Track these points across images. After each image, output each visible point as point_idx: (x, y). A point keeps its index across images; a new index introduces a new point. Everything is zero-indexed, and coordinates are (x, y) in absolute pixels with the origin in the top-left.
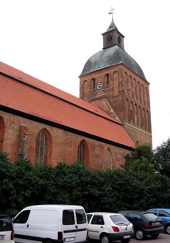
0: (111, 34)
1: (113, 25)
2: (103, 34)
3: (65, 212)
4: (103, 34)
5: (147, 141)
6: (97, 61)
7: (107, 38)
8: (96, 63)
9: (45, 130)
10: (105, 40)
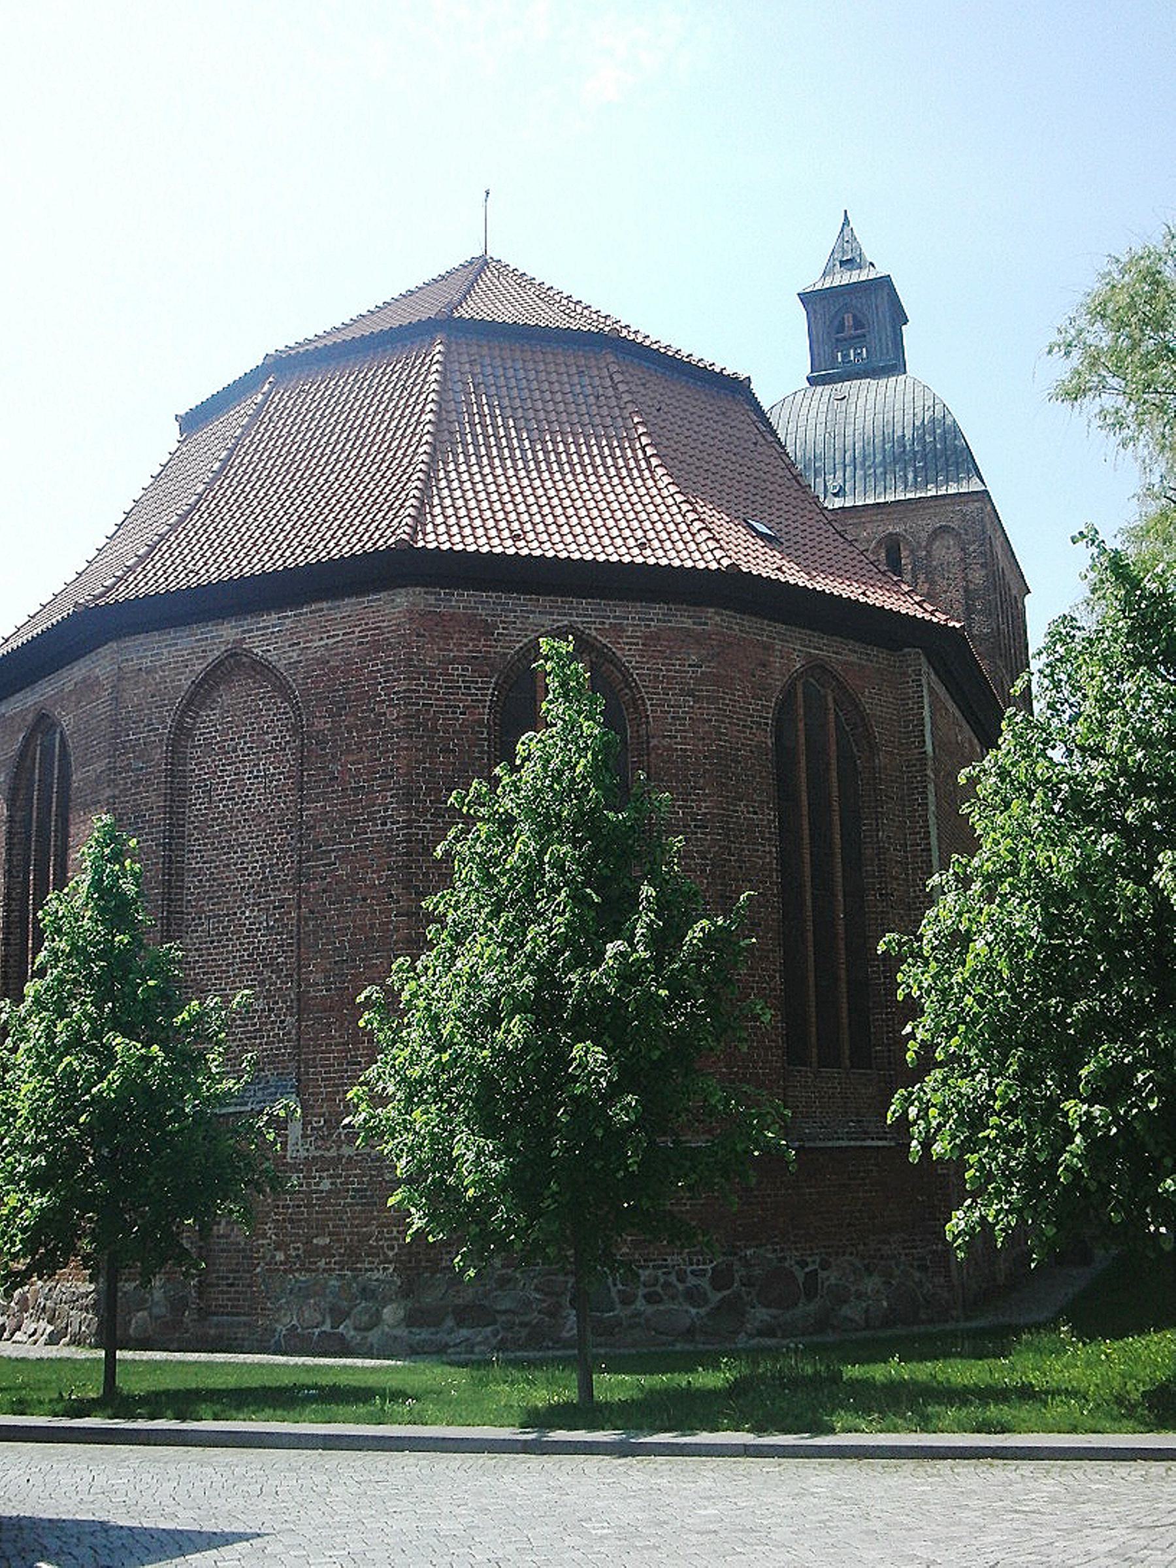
2: (806, 298)
4: (806, 298)
7: (834, 317)
9: (817, 669)
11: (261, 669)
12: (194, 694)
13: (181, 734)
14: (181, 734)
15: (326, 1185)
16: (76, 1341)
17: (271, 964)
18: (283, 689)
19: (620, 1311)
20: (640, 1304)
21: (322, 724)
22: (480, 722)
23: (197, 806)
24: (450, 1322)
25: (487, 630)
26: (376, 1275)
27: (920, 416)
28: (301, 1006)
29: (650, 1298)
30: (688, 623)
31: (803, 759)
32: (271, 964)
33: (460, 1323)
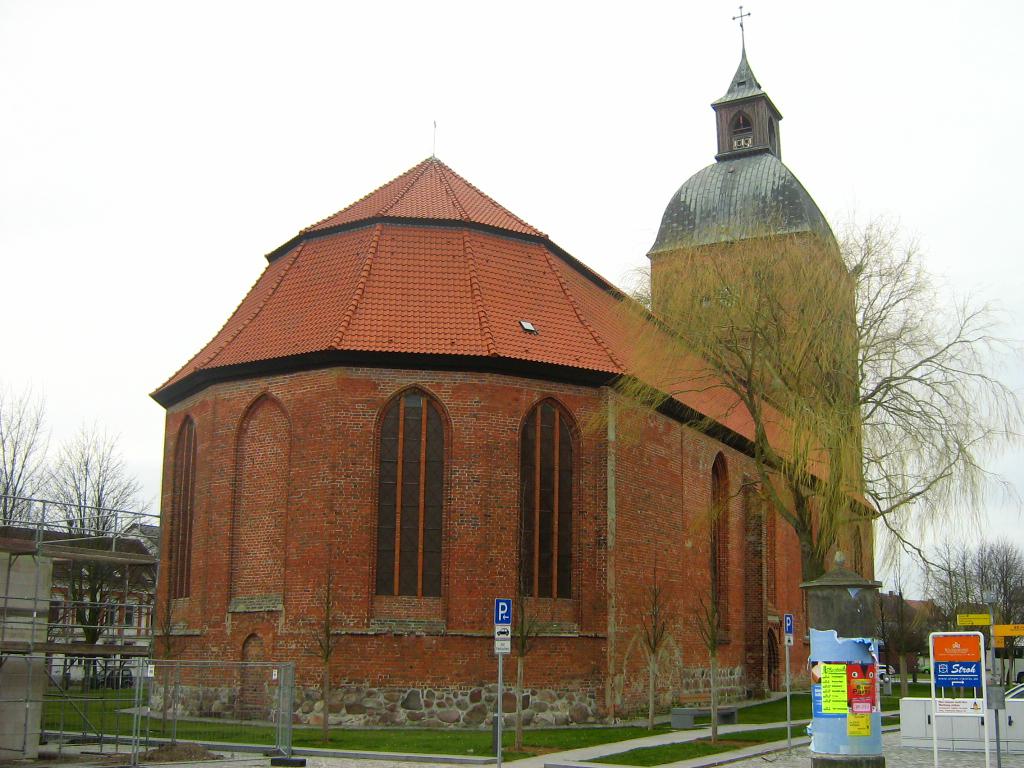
0: (747, 110)
1: (744, 77)
2: (716, 107)
3: (272, 760)
4: (716, 107)
5: (736, 721)
6: (714, 209)
7: (733, 119)
8: (709, 215)
9: (549, 400)
10: (726, 126)
11: (275, 402)
12: (248, 412)
13: (241, 431)
14: (241, 431)
15: (294, 646)
16: (739, 699)
17: (275, 543)
18: (284, 411)
19: (424, 710)
20: (435, 708)
21: (300, 430)
22: (370, 432)
23: (247, 465)
24: (344, 711)
25: (375, 386)
26: (312, 688)
27: (777, 183)
28: (286, 564)
29: (440, 705)
30: (476, 381)
31: (538, 445)
32: (275, 543)
33: (348, 712)
